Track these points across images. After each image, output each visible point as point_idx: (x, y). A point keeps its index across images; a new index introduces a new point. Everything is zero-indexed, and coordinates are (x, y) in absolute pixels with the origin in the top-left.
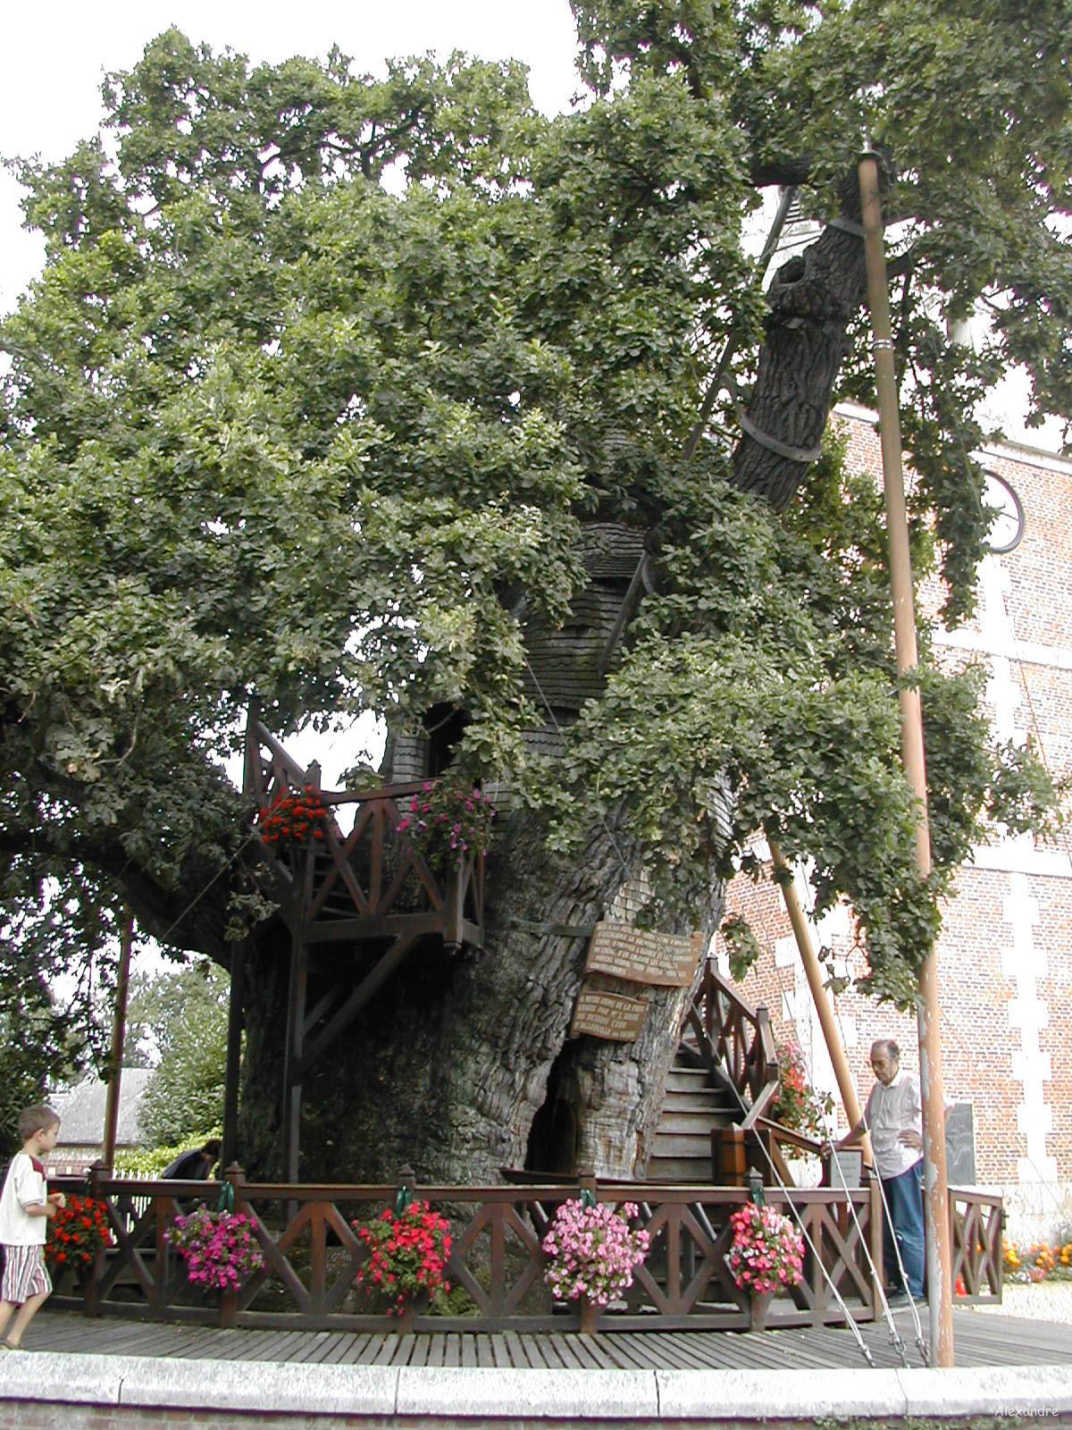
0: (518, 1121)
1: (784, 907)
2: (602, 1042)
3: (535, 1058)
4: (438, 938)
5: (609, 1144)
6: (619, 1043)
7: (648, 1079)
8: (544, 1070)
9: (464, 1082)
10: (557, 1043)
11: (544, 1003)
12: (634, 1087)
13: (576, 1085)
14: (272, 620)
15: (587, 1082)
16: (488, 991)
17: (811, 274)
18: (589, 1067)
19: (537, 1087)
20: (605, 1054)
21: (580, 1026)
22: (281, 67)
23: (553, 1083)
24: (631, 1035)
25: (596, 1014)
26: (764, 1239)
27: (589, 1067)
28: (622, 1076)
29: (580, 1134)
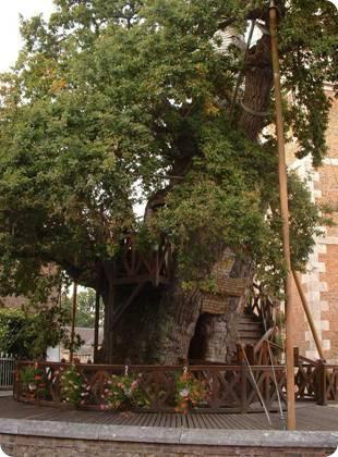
0: (184, 343)
1: (306, 320)
2: (212, 315)
3: (189, 321)
4: (150, 283)
5: (216, 349)
6: (219, 315)
7: (230, 327)
8: (193, 325)
9: (165, 329)
10: (196, 316)
11: (190, 303)
12: (224, 329)
13: (206, 329)
14: (106, 390)
15: (209, 329)
16: (172, 299)
17: (257, 51)
18: (209, 323)
19: (191, 329)
20: (215, 319)
21: (204, 310)
22: (20, 65)
23: (197, 329)
24: (222, 312)
25: (209, 306)
26: (91, 65)
27: (209, 323)
28: (221, 326)
29: (206, 345)
